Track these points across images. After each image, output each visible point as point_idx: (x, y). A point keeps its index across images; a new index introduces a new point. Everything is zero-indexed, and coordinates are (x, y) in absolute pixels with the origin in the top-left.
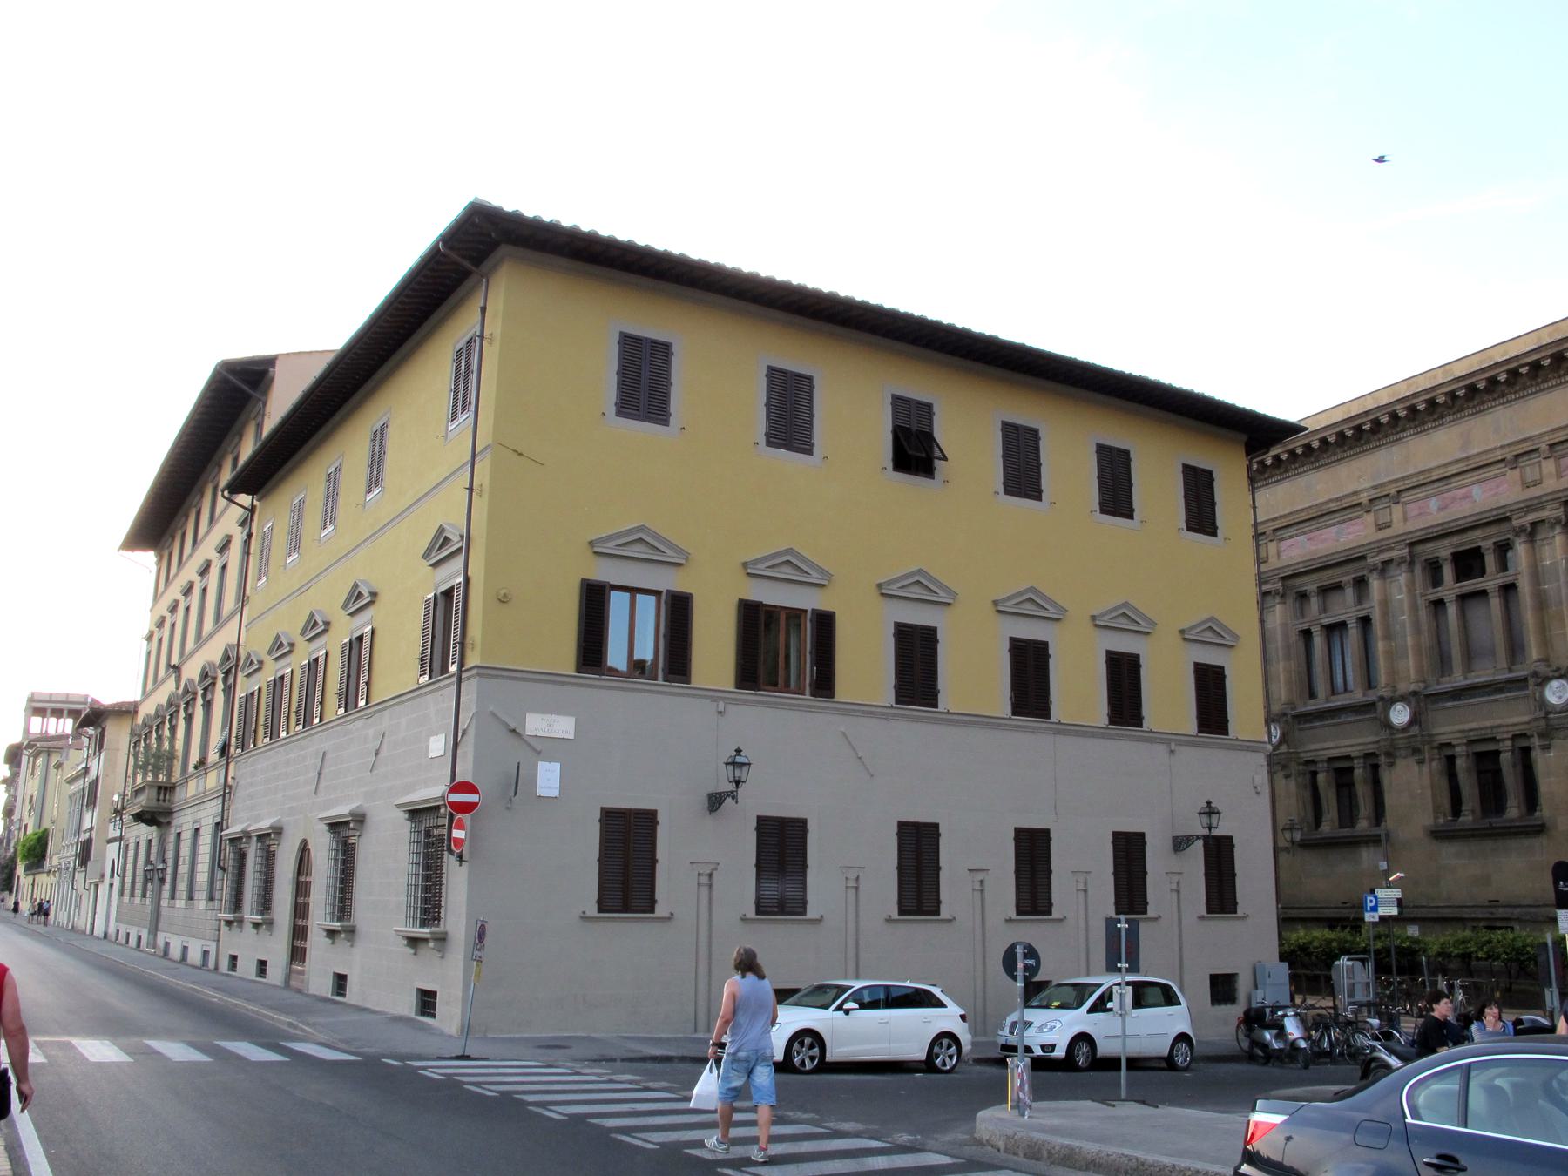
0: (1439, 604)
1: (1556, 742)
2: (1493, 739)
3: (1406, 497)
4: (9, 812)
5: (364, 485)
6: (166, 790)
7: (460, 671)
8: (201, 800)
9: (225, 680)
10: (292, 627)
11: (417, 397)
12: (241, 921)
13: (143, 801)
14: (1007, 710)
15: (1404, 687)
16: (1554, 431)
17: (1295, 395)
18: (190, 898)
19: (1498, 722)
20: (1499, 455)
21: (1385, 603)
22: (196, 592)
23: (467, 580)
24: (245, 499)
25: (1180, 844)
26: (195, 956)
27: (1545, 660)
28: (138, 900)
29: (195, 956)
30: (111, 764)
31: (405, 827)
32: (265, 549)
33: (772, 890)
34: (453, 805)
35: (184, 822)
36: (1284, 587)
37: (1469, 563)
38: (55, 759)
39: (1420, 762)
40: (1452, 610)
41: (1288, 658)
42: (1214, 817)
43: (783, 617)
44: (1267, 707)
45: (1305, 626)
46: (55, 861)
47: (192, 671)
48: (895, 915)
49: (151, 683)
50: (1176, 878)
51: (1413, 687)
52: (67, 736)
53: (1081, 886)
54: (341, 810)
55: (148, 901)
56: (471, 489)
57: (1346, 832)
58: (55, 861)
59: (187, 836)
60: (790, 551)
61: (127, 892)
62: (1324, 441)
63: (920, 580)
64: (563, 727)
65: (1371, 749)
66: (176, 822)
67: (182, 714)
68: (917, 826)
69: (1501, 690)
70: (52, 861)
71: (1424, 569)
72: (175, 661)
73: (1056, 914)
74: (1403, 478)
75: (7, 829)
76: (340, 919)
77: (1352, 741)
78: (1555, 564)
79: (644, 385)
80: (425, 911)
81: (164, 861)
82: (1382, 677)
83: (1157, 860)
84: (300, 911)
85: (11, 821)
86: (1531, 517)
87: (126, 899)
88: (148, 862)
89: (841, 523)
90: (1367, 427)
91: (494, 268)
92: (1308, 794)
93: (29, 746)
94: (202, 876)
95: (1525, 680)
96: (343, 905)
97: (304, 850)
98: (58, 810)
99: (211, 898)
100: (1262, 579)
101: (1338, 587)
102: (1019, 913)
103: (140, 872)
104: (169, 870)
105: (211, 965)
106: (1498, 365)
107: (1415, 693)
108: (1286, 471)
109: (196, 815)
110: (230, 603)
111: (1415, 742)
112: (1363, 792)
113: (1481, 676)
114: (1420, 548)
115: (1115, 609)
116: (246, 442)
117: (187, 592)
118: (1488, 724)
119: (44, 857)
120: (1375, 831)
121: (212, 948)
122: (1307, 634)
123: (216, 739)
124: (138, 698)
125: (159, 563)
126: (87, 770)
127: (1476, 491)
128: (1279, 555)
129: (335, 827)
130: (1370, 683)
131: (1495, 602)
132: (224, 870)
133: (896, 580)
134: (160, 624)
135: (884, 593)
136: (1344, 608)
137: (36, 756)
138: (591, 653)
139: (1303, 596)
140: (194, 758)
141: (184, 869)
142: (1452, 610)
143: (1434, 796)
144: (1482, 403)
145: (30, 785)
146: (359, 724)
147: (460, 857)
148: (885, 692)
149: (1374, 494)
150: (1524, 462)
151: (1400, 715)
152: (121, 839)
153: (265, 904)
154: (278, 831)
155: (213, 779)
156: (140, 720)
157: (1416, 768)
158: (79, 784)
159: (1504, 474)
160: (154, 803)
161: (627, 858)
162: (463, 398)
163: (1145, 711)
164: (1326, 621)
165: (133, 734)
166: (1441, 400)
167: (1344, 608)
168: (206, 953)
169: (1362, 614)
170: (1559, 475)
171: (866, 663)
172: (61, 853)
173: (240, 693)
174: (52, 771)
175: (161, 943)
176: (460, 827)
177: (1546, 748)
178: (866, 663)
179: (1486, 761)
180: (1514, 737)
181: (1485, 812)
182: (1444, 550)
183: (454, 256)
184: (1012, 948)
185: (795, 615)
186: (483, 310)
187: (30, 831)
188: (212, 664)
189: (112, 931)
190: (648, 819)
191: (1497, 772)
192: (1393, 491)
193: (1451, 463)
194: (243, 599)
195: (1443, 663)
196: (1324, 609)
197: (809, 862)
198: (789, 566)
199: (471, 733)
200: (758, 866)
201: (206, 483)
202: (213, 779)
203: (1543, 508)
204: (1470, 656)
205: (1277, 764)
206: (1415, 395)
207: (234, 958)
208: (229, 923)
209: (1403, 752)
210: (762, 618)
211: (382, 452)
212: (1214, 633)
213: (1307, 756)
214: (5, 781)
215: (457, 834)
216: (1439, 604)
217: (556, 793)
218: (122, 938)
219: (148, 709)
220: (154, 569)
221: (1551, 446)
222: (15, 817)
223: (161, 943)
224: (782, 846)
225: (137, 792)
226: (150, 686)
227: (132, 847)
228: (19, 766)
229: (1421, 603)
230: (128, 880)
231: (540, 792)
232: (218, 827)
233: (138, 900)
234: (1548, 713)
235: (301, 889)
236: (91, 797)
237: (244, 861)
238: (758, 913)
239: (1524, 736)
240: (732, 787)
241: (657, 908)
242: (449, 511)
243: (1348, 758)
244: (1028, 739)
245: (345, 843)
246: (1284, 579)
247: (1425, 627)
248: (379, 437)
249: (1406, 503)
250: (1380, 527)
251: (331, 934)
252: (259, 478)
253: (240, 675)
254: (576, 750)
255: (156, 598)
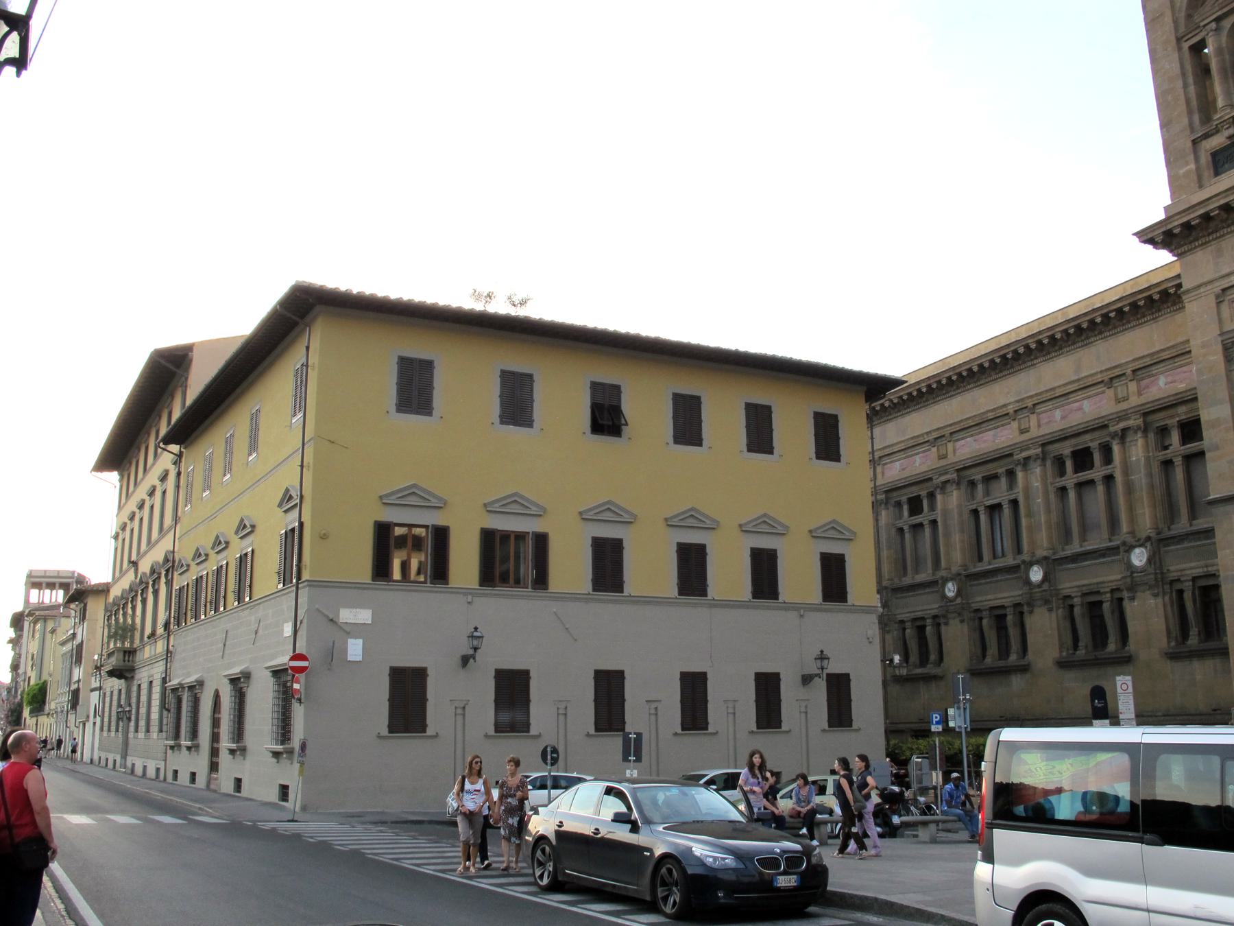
0: (1063, 490)
1: (1139, 594)
2: (1098, 592)
3: (1040, 409)
4: (15, 667)
5: (246, 451)
6: (130, 653)
7: (297, 583)
8: (152, 661)
9: (166, 575)
10: (207, 543)
11: (273, 396)
12: (179, 746)
13: (113, 662)
14: (675, 592)
15: (1041, 553)
16: (1134, 360)
17: (900, 356)
18: (148, 731)
19: (1100, 579)
20: (1099, 378)
21: (1027, 489)
22: (158, 494)
23: (301, 525)
24: (174, 448)
25: (807, 680)
26: (151, 773)
27: (1132, 533)
28: (113, 734)
29: (151, 773)
30: (92, 631)
31: (270, 681)
32: (190, 485)
33: (506, 717)
34: (293, 668)
35: (142, 676)
36: (887, 497)
37: (1082, 459)
38: (50, 625)
39: (1050, 610)
40: (1072, 495)
41: (962, 531)
42: (826, 662)
43: (512, 538)
44: (879, 582)
45: (974, 507)
46: (53, 706)
47: (145, 567)
48: (592, 731)
49: (118, 574)
50: (804, 704)
51: (1045, 553)
52: (59, 606)
53: (803, 709)
54: (236, 670)
55: (120, 734)
56: (302, 466)
57: (1002, 663)
58: (53, 706)
59: (145, 686)
60: (516, 494)
61: (106, 728)
62: (960, 374)
63: (609, 507)
64: (364, 616)
65: (1018, 600)
66: (137, 677)
67: (139, 598)
68: (608, 673)
69: (1103, 556)
70: (51, 705)
71: (1053, 463)
72: (134, 558)
73: (711, 729)
74: (1036, 395)
75: (14, 679)
76: (282, 744)
77: (1004, 594)
78: (1138, 460)
79: (415, 389)
80: (283, 735)
81: (130, 705)
82: (1025, 546)
83: (789, 693)
84: (215, 738)
85: (18, 675)
86: (1122, 425)
87: (105, 733)
88: (120, 705)
89: (555, 474)
90: (1009, 356)
91: (315, 318)
92: (977, 635)
93: (30, 614)
94: (155, 716)
95: (1118, 548)
96: (239, 732)
97: (217, 696)
98: (54, 666)
99: (161, 731)
100: (875, 492)
101: (995, 477)
102: (683, 729)
103: (114, 714)
104: (134, 712)
105: (162, 777)
106: (1094, 310)
107: (1046, 558)
108: (958, 388)
109: (149, 673)
110: (168, 521)
111: (1047, 595)
112: (1013, 633)
113: (1089, 546)
114: (1050, 448)
115: (759, 518)
116: (171, 410)
117: (152, 493)
118: (1095, 581)
119: (44, 702)
120: (1022, 662)
121: (161, 765)
122: (975, 512)
123: (162, 617)
124: (109, 580)
125: (121, 480)
126: (74, 635)
127: (1086, 405)
128: (954, 451)
129: (234, 681)
130: (1019, 550)
131: (1100, 488)
132: (169, 710)
133: (590, 510)
134: (124, 528)
135: (584, 517)
136: (1000, 492)
137: (35, 623)
138: (381, 570)
139: (972, 484)
140: (148, 631)
141: (143, 710)
142: (1072, 495)
143: (1060, 636)
144: (1088, 338)
145: (31, 646)
146: (246, 612)
147: (299, 700)
148: (584, 583)
149: (1017, 406)
150: (1116, 383)
151: (1036, 575)
152: (100, 688)
153: (194, 733)
154: (200, 683)
155: (160, 646)
156: (111, 600)
157: (1047, 614)
158: (68, 647)
159: (1103, 392)
160: (121, 663)
161: (407, 699)
162: (300, 403)
163: (781, 589)
164: (989, 503)
165: (106, 610)
166: (1058, 336)
167: (1000, 492)
168: (158, 769)
169: (1012, 497)
170: (1140, 394)
171: (571, 565)
172: (57, 700)
173: (176, 587)
174: (49, 636)
175: (129, 764)
176: (298, 682)
177: (1132, 599)
178: (571, 565)
179: (1094, 608)
180: (1112, 591)
181: (1095, 647)
182: (1066, 449)
183: (289, 315)
184: (545, 749)
185: (520, 537)
186: (308, 348)
187: (33, 682)
188: (157, 563)
189: (96, 758)
190: (419, 675)
191: (1102, 617)
192: (1030, 405)
193: (1067, 384)
194: (176, 520)
195: (1171, 512)
196: (987, 493)
197: (532, 697)
198: (514, 503)
199: (305, 621)
200: (496, 701)
201: (151, 427)
202: (160, 646)
203: (1129, 419)
204: (1084, 529)
205: (884, 623)
206: (1040, 332)
207: (176, 772)
208: (172, 748)
209: (1039, 603)
210: (498, 540)
211: (257, 429)
212: (835, 530)
213: (975, 606)
214: (11, 641)
215: (296, 686)
216: (1063, 490)
217: (359, 658)
218: (103, 763)
219: (116, 592)
220: (118, 485)
221: (1134, 371)
222: (21, 671)
223: (129, 764)
224: (512, 689)
225: (110, 655)
226: (117, 574)
227: (108, 694)
228: (22, 629)
229: (1051, 489)
230: (106, 719)
231: (349, 658)
232: (164, 681)
233: (113, 734)
234: (1132, 573)
235: (216, 723)
236: (78, 656)
237: (181, 703)
238: (496, 731)
239: (1118, 589)
240: (471, 652)
241: (428, 729)
242: (289, 478)
243: (1003, 607)
244: (692, 613)
245: (284, 685)
246: (958, 470)
247: (1053, 507)
248: (255, 418)
249: (1039, 414)
250: (1022, 432)
251: (232, 752)
252: (187, 432)
253: (176, 574)
254: (374, 628)
255: (120, 508)
